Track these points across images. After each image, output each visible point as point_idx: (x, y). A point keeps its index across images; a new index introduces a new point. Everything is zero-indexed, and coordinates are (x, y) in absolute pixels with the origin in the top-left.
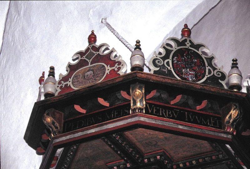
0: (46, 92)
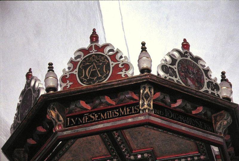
0: (47, 87)
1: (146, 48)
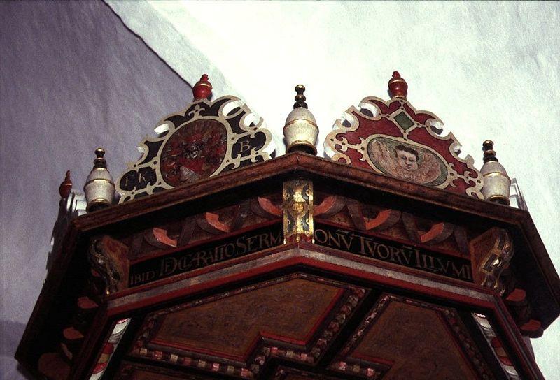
1: (304, 99)
